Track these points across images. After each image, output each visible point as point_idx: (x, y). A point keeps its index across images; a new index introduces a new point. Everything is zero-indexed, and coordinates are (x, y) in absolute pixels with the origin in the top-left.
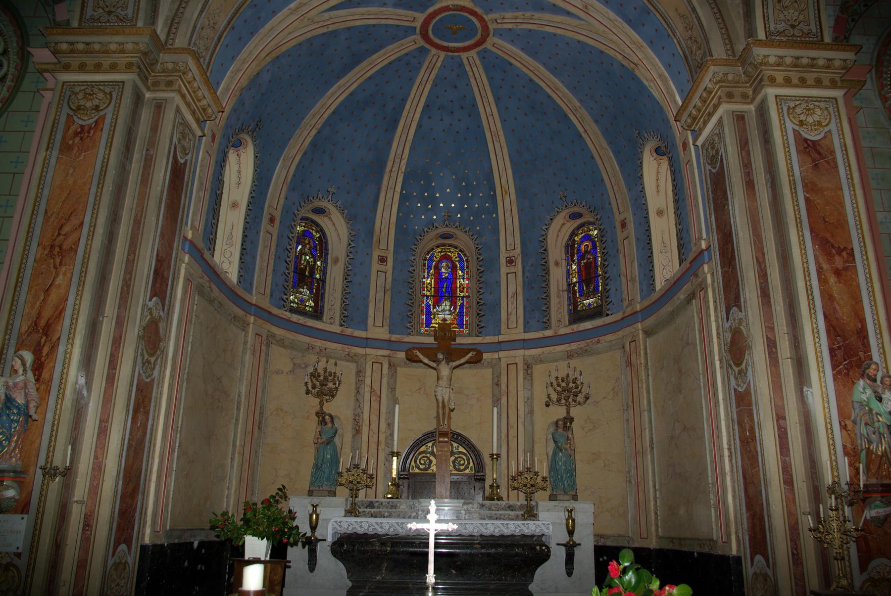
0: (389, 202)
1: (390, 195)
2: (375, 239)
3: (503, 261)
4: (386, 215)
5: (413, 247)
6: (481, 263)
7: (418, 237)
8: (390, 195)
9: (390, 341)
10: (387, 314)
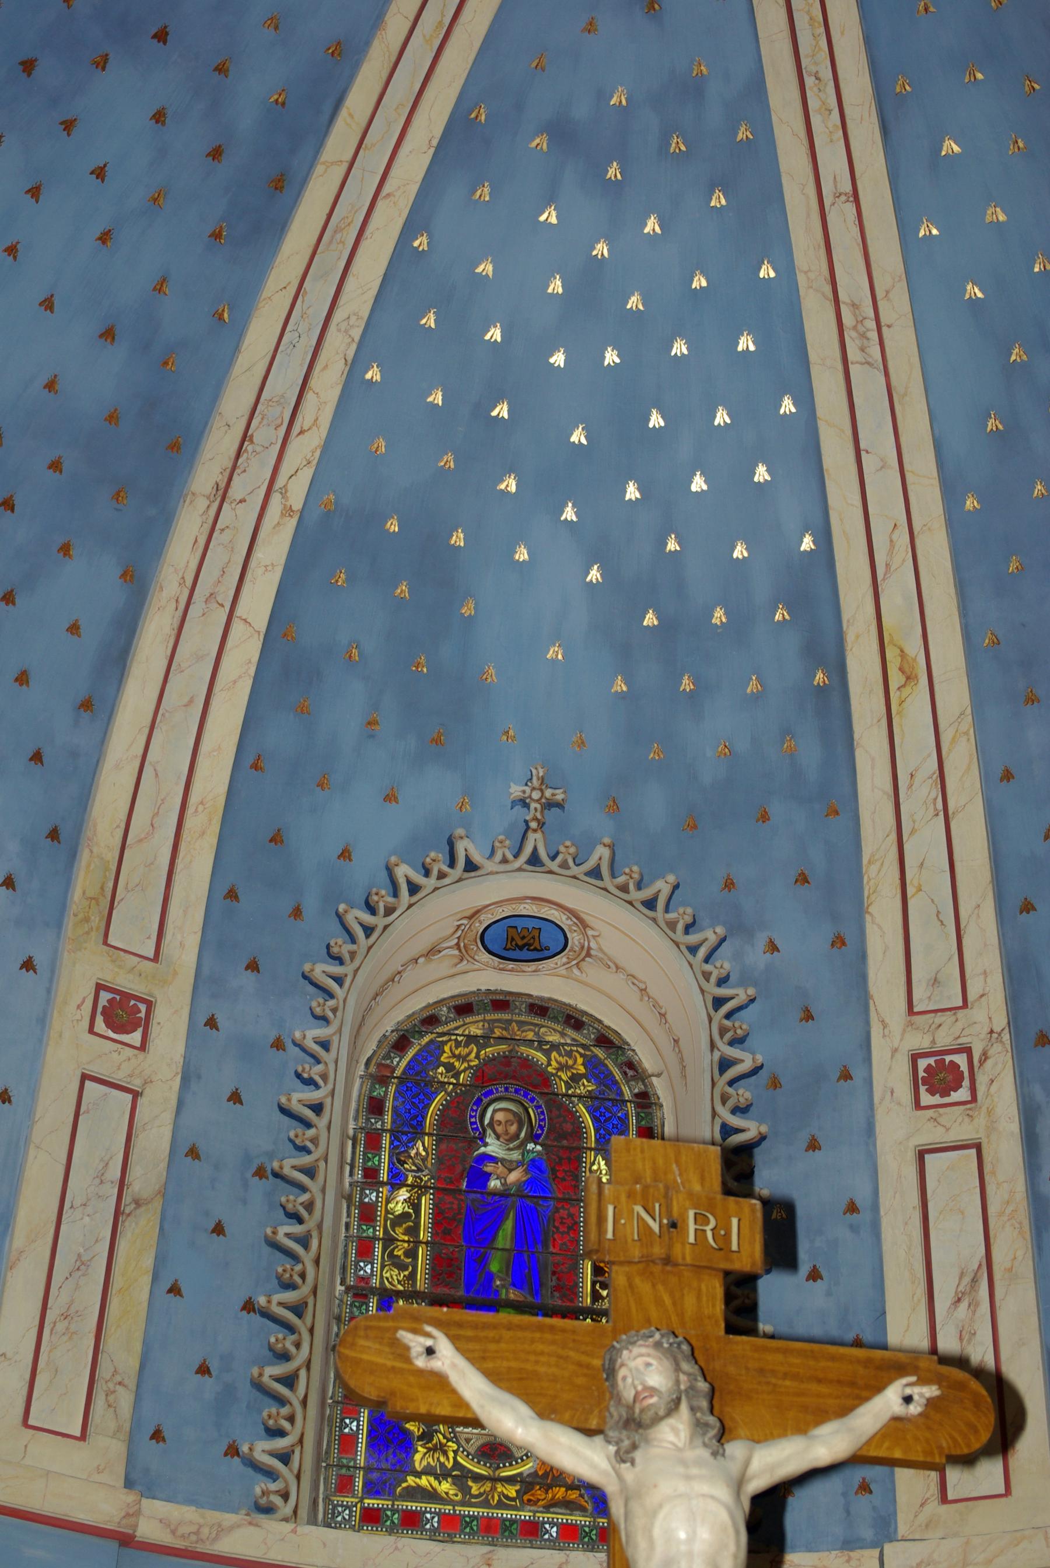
0: (189, 682)
1: (201, 637)
2: (86, 881)
3: (890, 1076)
4: (170, 755)
5: (321, 970)
6: (743, 1094)
7: (356, 916)
8: (201, 637)
9: (126, 1540)
10: (123, 1353)
